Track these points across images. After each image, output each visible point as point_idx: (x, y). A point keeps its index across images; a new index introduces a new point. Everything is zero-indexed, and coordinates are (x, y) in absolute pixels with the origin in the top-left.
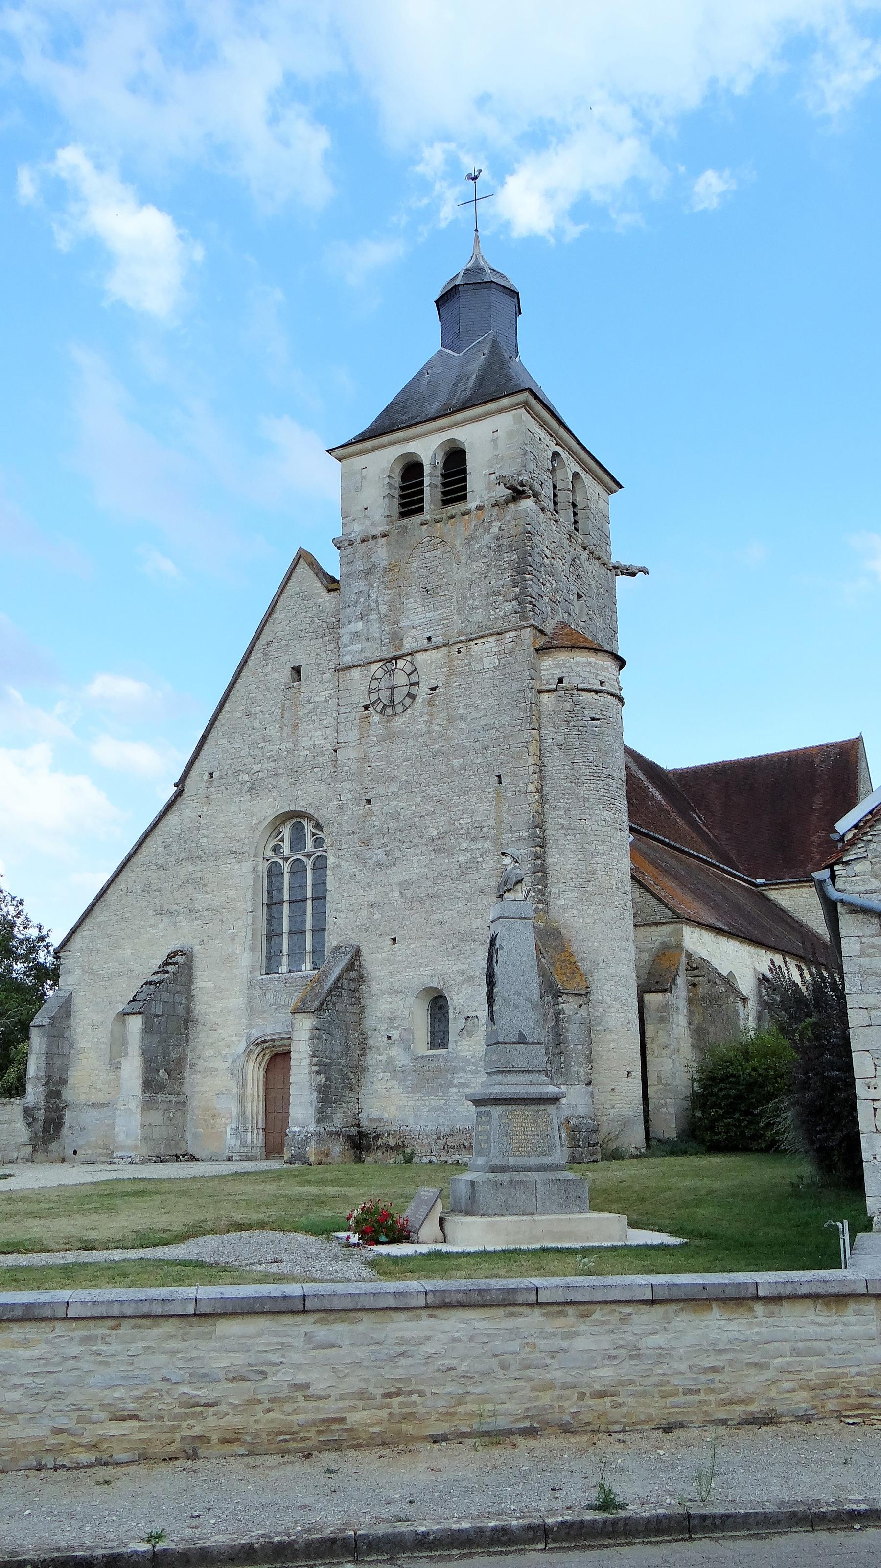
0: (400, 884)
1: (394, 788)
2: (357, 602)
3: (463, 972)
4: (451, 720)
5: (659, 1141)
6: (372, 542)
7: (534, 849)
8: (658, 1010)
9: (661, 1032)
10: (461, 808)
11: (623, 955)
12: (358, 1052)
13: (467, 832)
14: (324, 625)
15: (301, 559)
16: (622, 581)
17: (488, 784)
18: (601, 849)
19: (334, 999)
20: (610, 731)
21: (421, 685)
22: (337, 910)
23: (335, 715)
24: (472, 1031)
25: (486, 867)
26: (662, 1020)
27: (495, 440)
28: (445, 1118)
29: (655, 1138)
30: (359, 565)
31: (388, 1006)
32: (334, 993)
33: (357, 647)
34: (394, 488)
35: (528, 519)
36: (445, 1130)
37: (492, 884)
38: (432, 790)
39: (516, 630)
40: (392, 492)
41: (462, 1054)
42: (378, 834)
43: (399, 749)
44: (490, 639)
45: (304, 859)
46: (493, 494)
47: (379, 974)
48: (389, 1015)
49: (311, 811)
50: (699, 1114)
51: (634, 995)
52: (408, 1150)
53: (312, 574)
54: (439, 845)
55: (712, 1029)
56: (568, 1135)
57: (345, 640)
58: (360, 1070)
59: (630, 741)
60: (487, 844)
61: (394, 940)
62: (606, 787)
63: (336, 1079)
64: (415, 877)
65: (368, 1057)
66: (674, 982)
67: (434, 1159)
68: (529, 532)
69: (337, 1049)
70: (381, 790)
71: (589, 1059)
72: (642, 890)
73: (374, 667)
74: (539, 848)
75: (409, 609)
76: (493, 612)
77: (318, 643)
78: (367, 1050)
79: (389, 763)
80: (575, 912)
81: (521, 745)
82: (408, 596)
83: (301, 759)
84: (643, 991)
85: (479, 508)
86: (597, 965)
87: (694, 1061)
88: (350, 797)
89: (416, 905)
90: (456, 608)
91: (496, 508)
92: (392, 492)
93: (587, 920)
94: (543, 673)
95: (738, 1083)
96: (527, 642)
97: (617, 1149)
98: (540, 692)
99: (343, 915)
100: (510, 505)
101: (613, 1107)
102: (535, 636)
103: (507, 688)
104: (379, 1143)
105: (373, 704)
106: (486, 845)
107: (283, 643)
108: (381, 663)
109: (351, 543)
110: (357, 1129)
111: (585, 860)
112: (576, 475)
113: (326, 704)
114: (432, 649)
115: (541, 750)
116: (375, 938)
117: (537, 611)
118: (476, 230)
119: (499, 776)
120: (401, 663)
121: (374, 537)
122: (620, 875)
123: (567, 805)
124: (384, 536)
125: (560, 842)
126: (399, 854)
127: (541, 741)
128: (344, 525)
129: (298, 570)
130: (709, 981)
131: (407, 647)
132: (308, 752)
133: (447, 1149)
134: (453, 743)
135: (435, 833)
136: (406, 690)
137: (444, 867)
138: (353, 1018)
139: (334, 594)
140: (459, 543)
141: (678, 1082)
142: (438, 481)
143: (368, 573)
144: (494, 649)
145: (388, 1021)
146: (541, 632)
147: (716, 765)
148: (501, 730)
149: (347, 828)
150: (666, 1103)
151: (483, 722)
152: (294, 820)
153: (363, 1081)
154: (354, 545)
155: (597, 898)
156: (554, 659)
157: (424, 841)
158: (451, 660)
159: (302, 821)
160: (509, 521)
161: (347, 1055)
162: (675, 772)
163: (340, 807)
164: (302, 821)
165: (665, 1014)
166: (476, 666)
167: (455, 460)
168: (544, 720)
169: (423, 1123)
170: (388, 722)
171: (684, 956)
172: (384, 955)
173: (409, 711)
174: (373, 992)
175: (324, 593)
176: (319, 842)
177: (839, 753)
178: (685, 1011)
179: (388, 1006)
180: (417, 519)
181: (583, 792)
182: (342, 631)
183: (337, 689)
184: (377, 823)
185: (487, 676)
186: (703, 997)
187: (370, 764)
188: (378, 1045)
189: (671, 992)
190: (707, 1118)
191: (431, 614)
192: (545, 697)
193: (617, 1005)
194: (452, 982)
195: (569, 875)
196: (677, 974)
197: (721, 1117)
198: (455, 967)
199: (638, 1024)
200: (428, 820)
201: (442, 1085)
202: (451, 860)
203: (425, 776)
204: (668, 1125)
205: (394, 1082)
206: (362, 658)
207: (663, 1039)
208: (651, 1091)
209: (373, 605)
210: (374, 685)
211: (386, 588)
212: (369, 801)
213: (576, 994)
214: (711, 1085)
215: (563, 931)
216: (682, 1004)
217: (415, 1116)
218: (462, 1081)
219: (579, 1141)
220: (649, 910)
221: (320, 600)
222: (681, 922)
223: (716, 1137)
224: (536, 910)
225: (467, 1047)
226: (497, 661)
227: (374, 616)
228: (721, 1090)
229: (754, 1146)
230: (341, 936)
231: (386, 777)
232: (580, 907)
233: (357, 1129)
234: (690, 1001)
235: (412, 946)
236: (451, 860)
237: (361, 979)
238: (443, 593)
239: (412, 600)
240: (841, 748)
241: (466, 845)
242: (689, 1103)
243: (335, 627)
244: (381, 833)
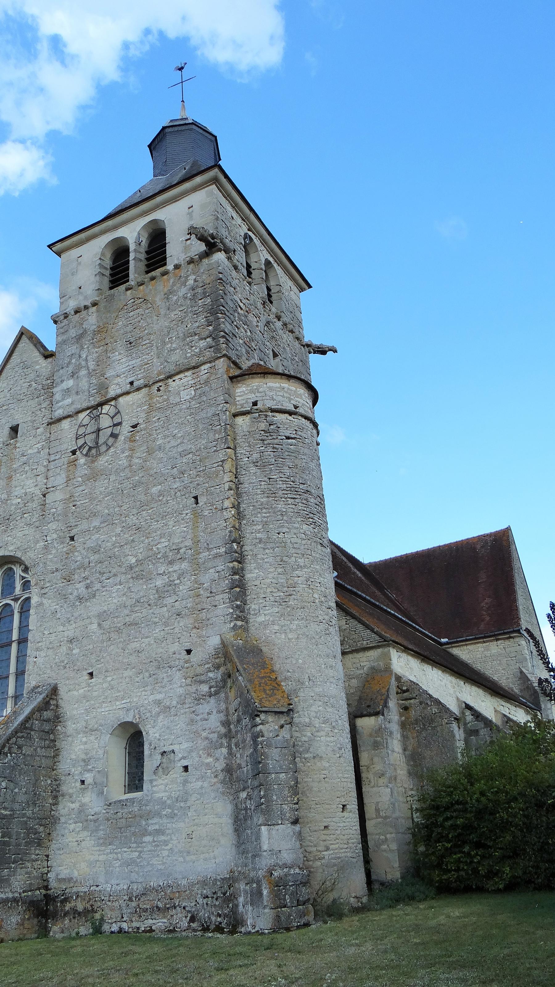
0: (99, 616)
1: (96, 523)
2: (69, 363)
3: (158, 703)
4: (150, 452)
5: (382, 884)
6: (84, 313)
7: (231, 565)
8: (371, 735)
9: (376, 759)
10: (159, 532)
11: (331, 672)
12: (51, 801)
13: (165, 556)
14: (40, 387)
15: (24, 336)
16: (314, 358)
17: (185, 507)
18: (301, 561)
19: (21, 741)
20: (306, 451)
21: (124, 424)
22: (37, 649)
23: (45, 464)
24: (168, 768)
25: (183, 589)
26: (376, 745)
27: (190, 215)
28: (137, 873)
29: (376, 880)
30: (73, 333)
31: (82, 747)
32: (19, 734)
33: (69, 401)
34: (106, 268)
35: (220, 268)
36: (137, 888)
37: (189, 605)
38: (132, 520)
39: (210, 362)
40: (103, 271)
41: (157, 795)
42: (79, 569)
43: (101, 486)
44: (186, 374)
45: (12, 603)
46: (189, 255)
47: (75, 712)
48: (83, 756)
49: (19, 554)
50: (422, 849)
51: (345, 717)
52: (97, 916)
53: (32, 347)
54: (138, 573)
55: (427, 753)
56: (271, 892)
57: (57, 397)
58: (49, 821)
59: (337, 535)
60: (185, 565)
61: (91, 674)
62: (304, 502)
63: (18, 834)
64: (113, 607)
65: (60, 807)
66: (386, 705)
67: (125, 926)
68: (221, 279)
69: (22, 798)
70: (84, 525)
71: (295, 789)
72: (348, 618)
73: (82, 416)
74: (235, 563)
75: (114, 361)
76: (189, 351)
77: (33, 403)
78: (60, 799)
79: (92, 499)
80: (276, 627)
81: (216, 465)
82: (114, 350)
83: (13, 507)
84: (353, 717)
85: (177, 267)
86: (303, 683)
87: (412, 789)
88: (55, 536)
89: (114, 636)
90: (156, 352)
91: (191, 266)
92: (103, 271)
93: (290, 636)
94: (238, 399)
95: (465, 811)
96: (221, 371)
97: (334, 900)
98: (235, 415)
99: (43, 654)
100: (203, 260)
101: (328, 849)
102: (229, 366)
103: (203, 415)
104: (67, 908)
105: (80, 448)
106: (183, 566)
107: (4, 408)
108: (88, 411)
109: (66, 316)
110: (43, 892)
111: (285, 573)
112: (268, 263)
113: (38, 455)
114: (134, 392)
115: (236, 469)
116: (72, 674)
117: (230, 345)
118: (183, 101)
119: (196, 498)
120: (106, 408)
121: (86, 308)
122: (323, 589)
123: (265, 519)
124: (94, 304)
125: (259, 556)
126: (97, 586)
127: (236, 460)
128: (61, 303)
129: (20, 345)
130: (421, 703)
131: (112, 393)
132: (19, 500)
133: (139, 912)
134: (152, 472)
135: (134, 560)
136: (109, 431)
137: (141, 594)
138: (45, 762)
139: (50, 360)
140: (159, 300)
141: (397, 814)
142: (143, 256)
143: (79, 338)
144: (190, 382)
145: (82, 764)
146: (235, 363)
147: (401, 557)
148: (197, 453)
149: (51, 566)
150: (386, 839)
151: (180, 449)
152: (6, 567)
153: (54, 834)
154: (70, 317)
155: (300, 612)
156: (248, 386)
157: (123, 570)
158: (151, 399)
159: (13, 567)
160: (203, 273)
161: (35, 804)
162: (371, 564)
163: (46, 547)
164: (13, 567)
165: (379, 739)
166: (173, 400)
167: (157, 238)
168: (240, 440)
169: (114, 882)
170: (93, 462)
171: (393, 679)
172: (81, 691)
173: (112, 450)
174: (69, 733)
175: (41, 360)
176: (26, 585)
177: (495, 540)
178: (399, 736)
179: (82, 747)
180: (122, 287)
181: (281, 506)
182: (55, 390)
183: (49, 440)
184: (79, 558)
185: (184, 406)
186: (416, 720)
187: (74, 503)
188: (71, 791)
189: (383, 715)
190: (433, 853)
191: (134, 362)
192: (240, 420)
193: (327, 728)
194: (148, 715)
195: (269, 590)
196: (388, 696)
197: (449, 852)
198: (152, 698)
199: (351, 749)
200: (127, 549)
201: (134, 834)
202: (149, 586)
203: (125, 507)
204: (391, 864)
205: (86, 833)
206: (72, 409)
207: (378, 767)
208: (370, 825)
209: (83, 363)
210: (81, 431)
211: (95, 347)
212: (72, 538)
213: (276, 713)
214: (435, 815)
215: (264, 649)
216: (395, 727)
217: (106, 873)
218: (157, 827)
219: (285, 899)
220: (356, 636)
221: (37, 367)
222: (388, 646)
223: (445, 877)
224: (235, 628)
225: (162, 787)
226: (193, 392)
227: (83, 372)
228: (447, 819)
229: (490, 885)
230: (40, 675)
231: (88, 514)
232: (282, 622)
233: (43, 892)
234: (403, 725)
235: (109, 679)
236: (149, 586)
237: (57, 719)
238: (144, 343)
239: (117, 353)
240: (495, 536)
241: (163, 568)
242: (411, 836)
243: (48, 389)
244: (82, 567)
